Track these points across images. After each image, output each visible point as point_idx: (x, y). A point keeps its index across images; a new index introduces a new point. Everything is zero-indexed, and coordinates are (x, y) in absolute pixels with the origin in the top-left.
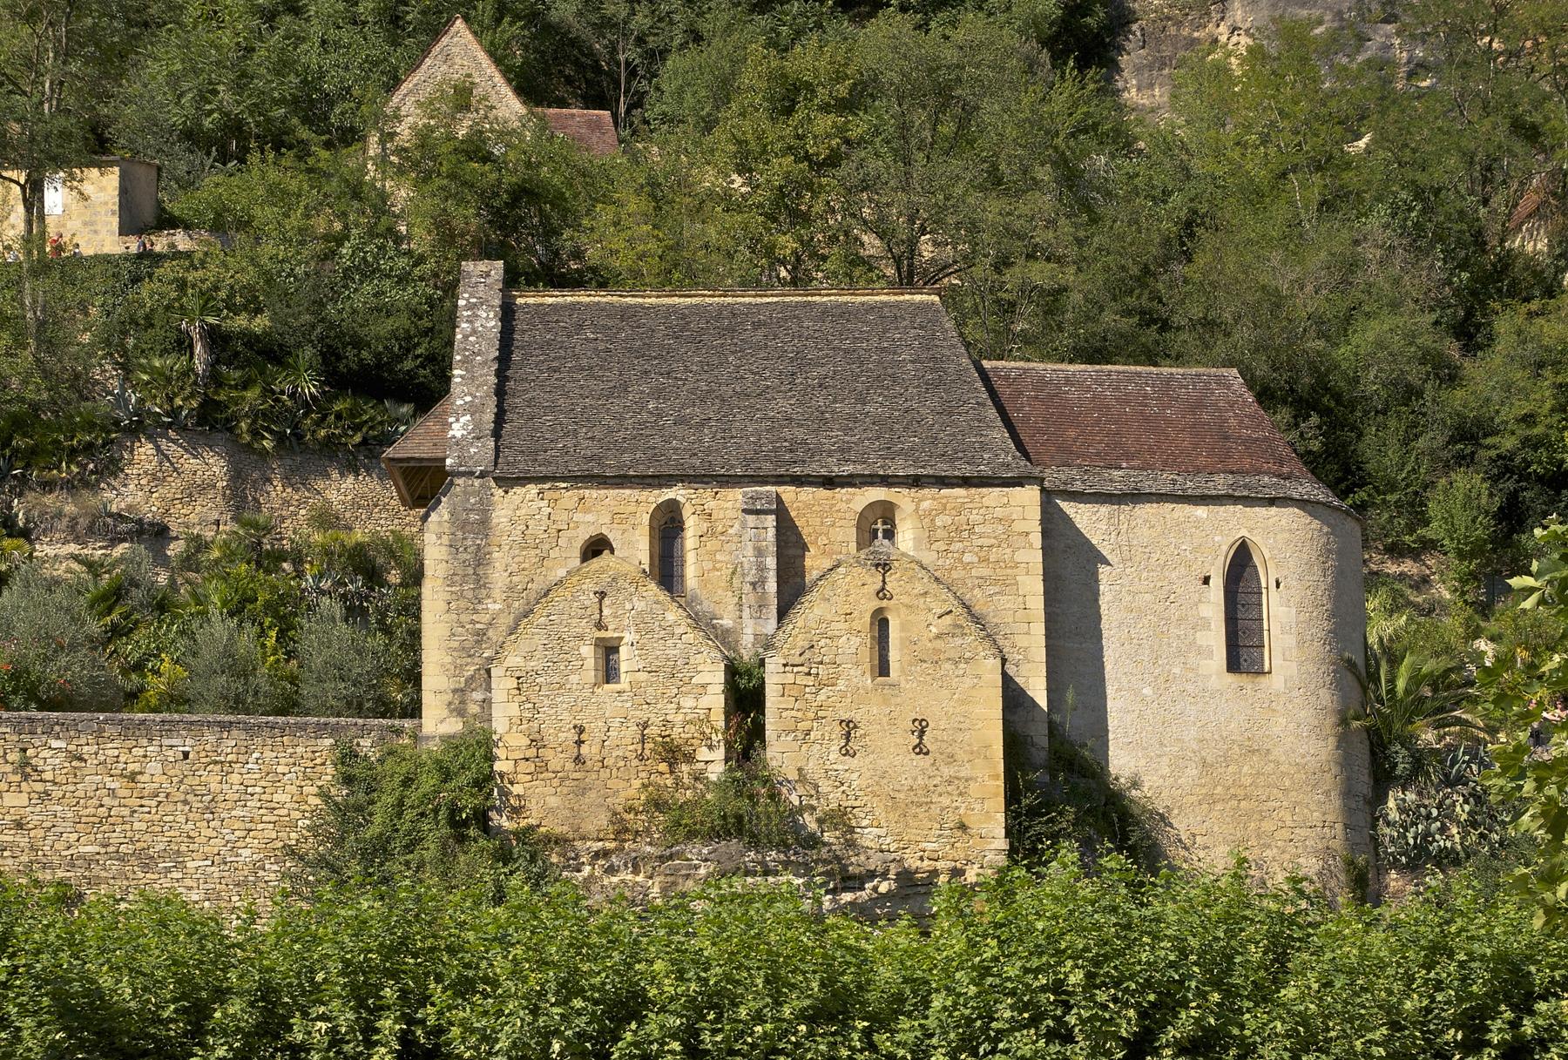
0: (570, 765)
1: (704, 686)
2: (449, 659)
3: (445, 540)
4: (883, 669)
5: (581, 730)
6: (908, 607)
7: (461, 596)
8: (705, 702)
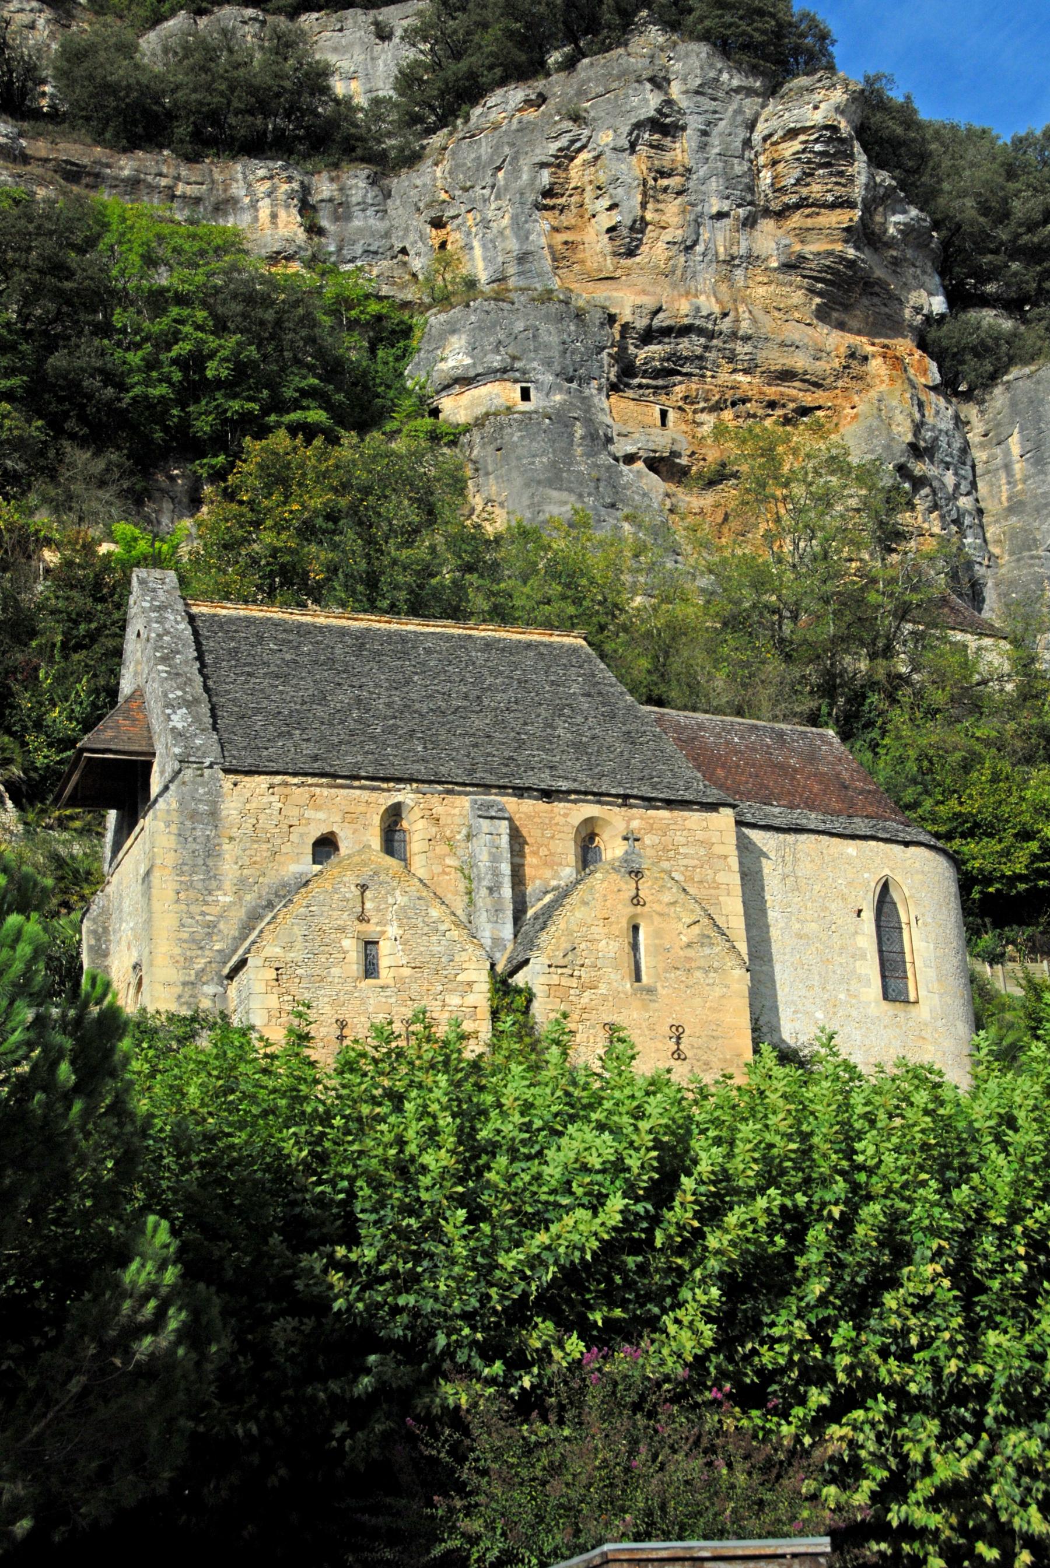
2: (177, 951)
3: (174, 828)
4: (638, 979)
5: (342, 1025)
6: (661, 915)
7: (190, 886)
8: (471, 999)
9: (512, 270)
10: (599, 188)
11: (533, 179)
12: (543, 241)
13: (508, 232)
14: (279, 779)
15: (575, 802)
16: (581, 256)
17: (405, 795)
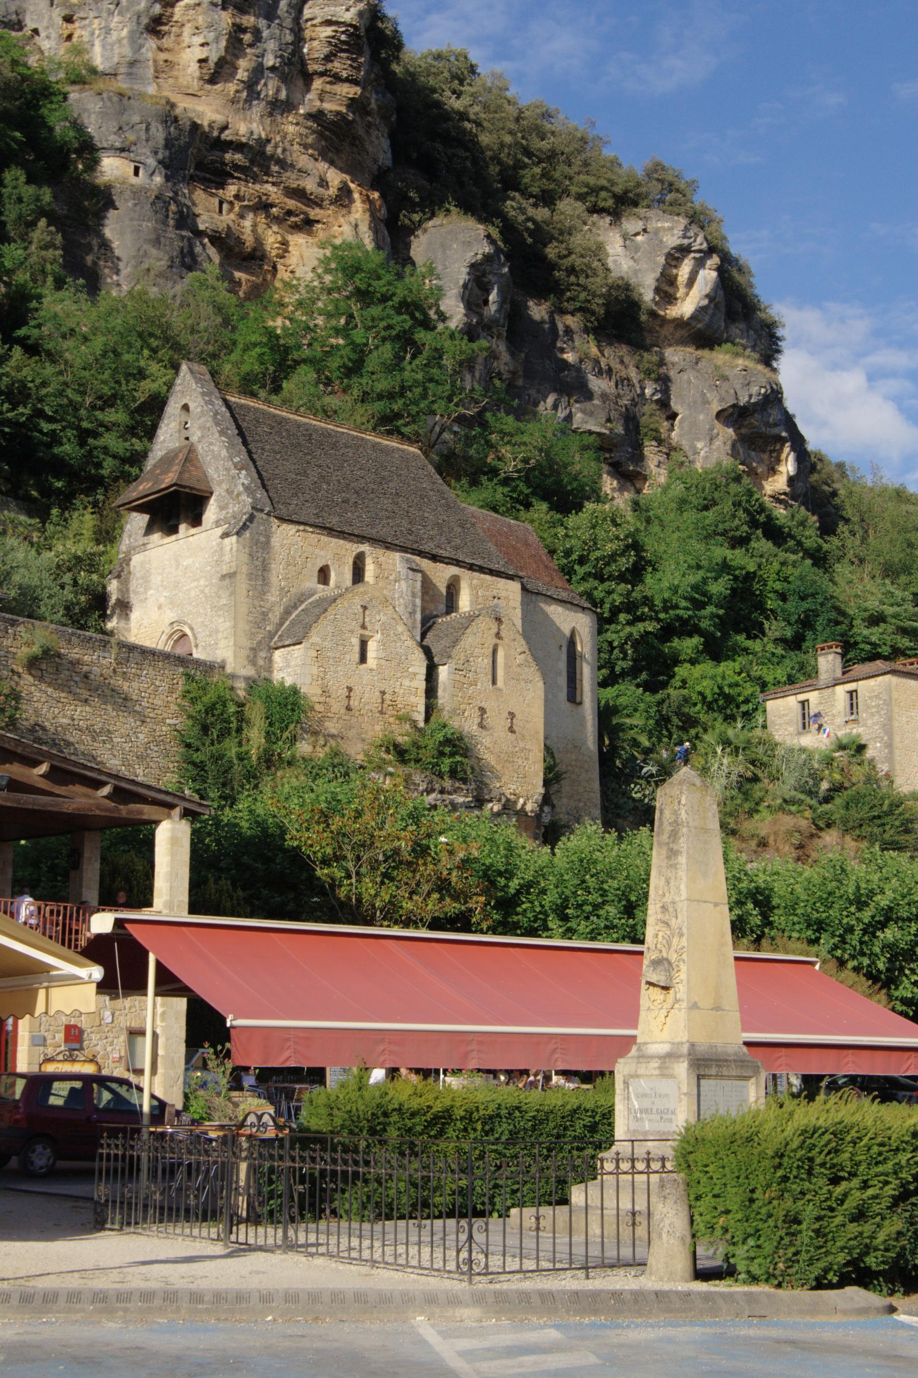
0: (343, 711)
1: (415, 674)
2: (247, 628)
3: (247, 550)
4: (494, 682)
5: (350, 689)
7: (255, 589)
9: (123, 70)
10: (197, 28)
11: (148, 9)
12: (150, 55)
13: (125, 42)
14: (302, 528)
15: (447, 564)
16: (176, 73)
17: (365, 548)
